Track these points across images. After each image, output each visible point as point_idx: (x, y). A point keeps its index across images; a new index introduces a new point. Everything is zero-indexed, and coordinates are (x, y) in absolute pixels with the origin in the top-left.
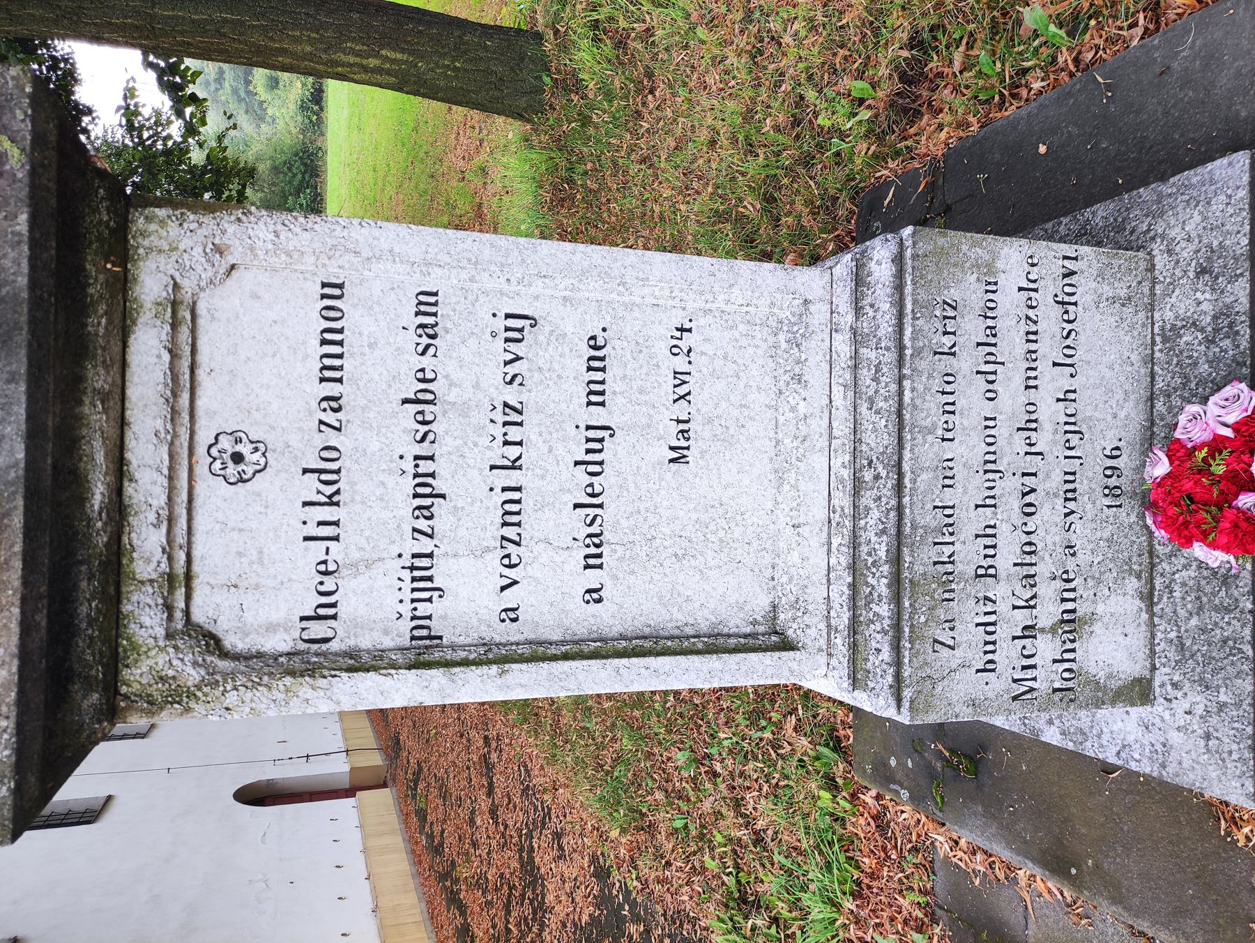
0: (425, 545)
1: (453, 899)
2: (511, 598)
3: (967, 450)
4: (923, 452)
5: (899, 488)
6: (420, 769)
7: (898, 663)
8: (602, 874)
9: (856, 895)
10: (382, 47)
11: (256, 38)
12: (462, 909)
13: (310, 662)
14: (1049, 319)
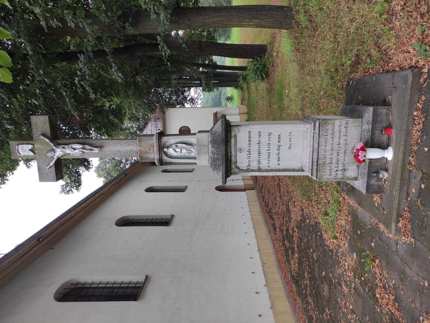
0: (259, 159)
1: (271, 218)
2: (269, 164)
3: (329, 148)
4: (322, 148)
5: (318, 153)
6: (263, 186)
7: (317, 174)
8: (302, 210)
9: (339, 211)
10: (253, 19)
11: (226, 23)
12: (273, 219)
13: (248, 170)
14: (343, 130)
